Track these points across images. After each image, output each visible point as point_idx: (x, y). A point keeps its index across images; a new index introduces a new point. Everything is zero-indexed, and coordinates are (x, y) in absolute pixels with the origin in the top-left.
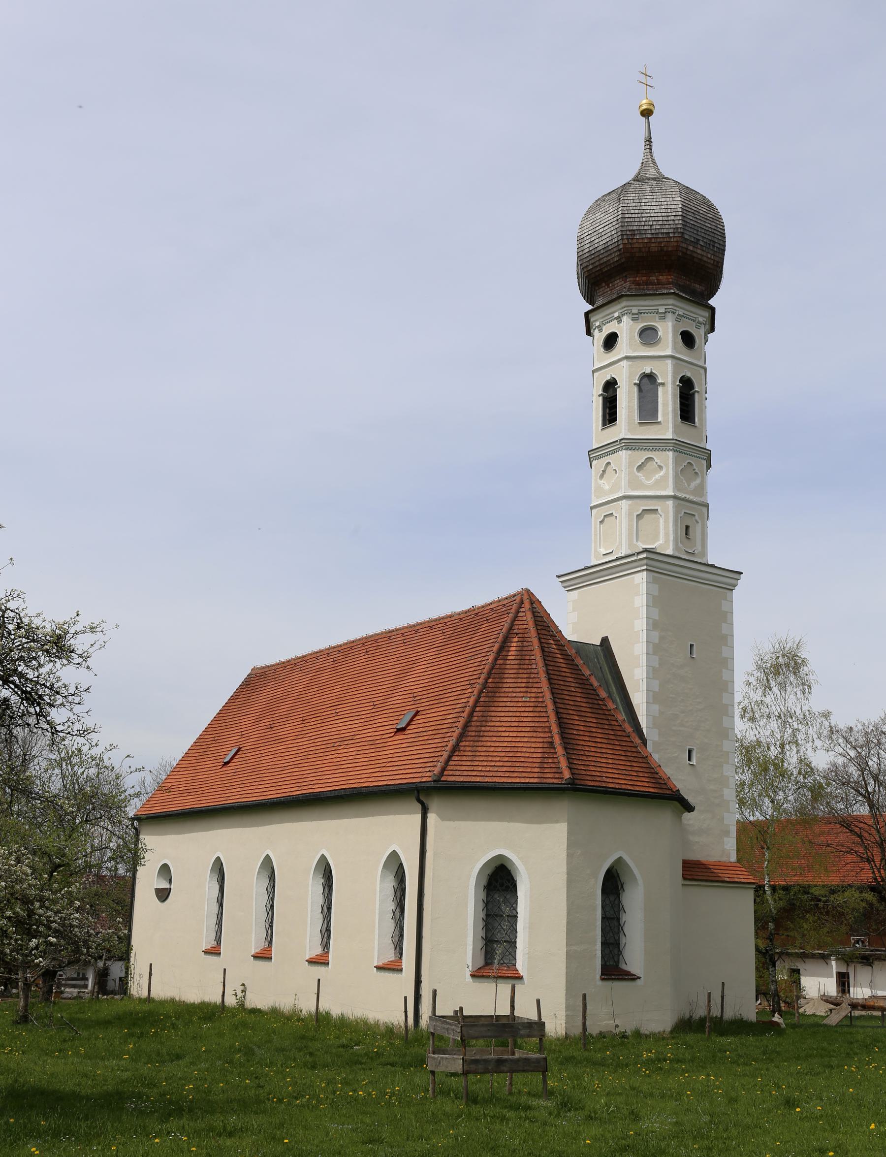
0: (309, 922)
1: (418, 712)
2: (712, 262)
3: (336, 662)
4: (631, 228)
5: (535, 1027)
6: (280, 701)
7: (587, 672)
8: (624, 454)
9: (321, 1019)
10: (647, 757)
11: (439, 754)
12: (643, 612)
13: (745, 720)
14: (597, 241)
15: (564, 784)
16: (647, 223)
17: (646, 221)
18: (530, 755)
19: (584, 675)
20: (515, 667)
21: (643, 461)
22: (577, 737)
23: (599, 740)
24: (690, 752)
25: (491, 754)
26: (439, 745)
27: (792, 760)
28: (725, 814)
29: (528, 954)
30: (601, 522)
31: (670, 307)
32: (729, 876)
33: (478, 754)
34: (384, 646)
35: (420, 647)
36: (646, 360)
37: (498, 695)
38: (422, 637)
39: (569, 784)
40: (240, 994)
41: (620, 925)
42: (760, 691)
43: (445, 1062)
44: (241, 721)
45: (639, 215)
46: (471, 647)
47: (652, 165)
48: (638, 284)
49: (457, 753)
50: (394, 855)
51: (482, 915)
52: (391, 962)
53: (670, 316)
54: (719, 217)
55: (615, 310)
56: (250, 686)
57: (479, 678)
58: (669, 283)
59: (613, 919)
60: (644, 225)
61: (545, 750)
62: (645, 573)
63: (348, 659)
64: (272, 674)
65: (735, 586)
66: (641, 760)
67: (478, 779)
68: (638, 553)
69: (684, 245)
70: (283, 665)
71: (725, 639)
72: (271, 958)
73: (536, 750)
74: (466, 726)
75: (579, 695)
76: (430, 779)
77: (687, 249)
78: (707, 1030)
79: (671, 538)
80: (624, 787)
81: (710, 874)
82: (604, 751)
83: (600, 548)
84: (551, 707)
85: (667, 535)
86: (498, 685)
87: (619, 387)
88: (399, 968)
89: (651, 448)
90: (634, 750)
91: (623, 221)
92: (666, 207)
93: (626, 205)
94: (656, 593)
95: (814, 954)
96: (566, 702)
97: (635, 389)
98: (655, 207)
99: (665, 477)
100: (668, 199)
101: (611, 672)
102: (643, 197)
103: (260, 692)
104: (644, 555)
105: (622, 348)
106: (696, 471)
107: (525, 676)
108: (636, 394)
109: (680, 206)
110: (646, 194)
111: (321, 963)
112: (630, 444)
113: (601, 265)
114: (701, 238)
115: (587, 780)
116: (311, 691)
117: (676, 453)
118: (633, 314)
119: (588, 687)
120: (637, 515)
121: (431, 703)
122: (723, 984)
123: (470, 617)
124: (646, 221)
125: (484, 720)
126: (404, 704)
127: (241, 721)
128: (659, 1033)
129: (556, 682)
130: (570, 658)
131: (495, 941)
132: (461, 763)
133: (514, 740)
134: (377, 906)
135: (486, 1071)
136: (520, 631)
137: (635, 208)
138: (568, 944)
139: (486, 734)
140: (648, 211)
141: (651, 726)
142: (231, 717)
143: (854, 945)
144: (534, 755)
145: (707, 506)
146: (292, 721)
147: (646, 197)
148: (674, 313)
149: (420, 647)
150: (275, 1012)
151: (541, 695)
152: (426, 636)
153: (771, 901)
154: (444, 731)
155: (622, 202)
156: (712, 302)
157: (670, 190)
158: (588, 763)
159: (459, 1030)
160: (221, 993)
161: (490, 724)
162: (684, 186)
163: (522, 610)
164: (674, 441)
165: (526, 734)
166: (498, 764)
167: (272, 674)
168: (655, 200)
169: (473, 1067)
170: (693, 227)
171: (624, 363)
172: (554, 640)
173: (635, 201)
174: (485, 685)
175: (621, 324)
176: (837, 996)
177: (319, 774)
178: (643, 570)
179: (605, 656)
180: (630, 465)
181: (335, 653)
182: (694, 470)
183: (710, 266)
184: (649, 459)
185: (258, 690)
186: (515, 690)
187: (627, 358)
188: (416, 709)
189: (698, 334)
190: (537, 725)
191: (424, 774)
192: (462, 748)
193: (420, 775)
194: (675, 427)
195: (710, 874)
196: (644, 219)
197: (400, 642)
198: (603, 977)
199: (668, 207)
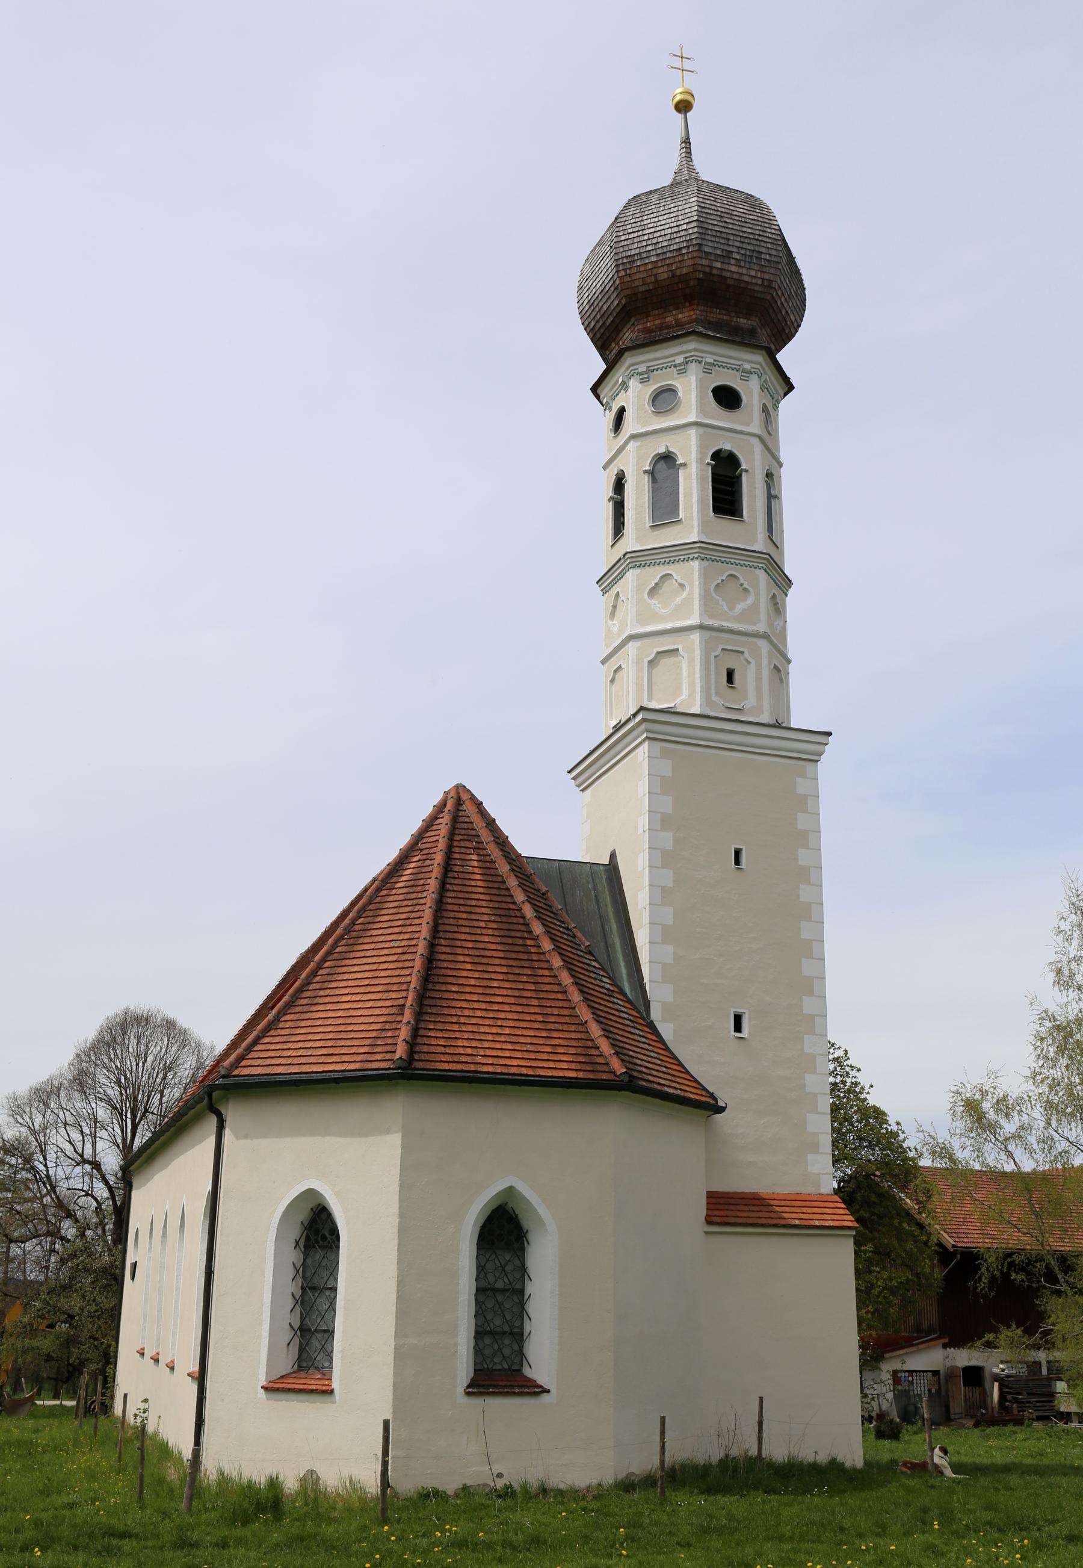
2: (760, 282)
4: (629, 253)
10: (586, 1022)
15: (393, 1069)
16: (649, 242)
17: (649, 239)
19: (514, 903)
21: (657, 580)
28: (807, 1115)
31: (692, 353)
36: (658, 435)
39: (399, 1068)
53: (692, 367)
60: (646, 246)
62: (646, 744)
65: (820, 754)
69: (705, 262)
77: (711, 267)
79: (698, 689)
85: (691, 685)
89: (667, 560)
92: (675, 214)
99: (688, 601)
106: (744, 586)
108: (647, 487)
114: (735, 250)
115: (441, 1061)
117: (705, 563)
120: (650, 662)
124: (649, 239)
138: (400, 1332)
140: (652, 225)
162: (714, 184)
170: (718, 234)
173: (635, 216)
178: (644, 740)
182: (742, 585)
183: (757, 288)
184: (667, 576)
194: (704, 526)
198: (470, 1390)
199: (680, 213)
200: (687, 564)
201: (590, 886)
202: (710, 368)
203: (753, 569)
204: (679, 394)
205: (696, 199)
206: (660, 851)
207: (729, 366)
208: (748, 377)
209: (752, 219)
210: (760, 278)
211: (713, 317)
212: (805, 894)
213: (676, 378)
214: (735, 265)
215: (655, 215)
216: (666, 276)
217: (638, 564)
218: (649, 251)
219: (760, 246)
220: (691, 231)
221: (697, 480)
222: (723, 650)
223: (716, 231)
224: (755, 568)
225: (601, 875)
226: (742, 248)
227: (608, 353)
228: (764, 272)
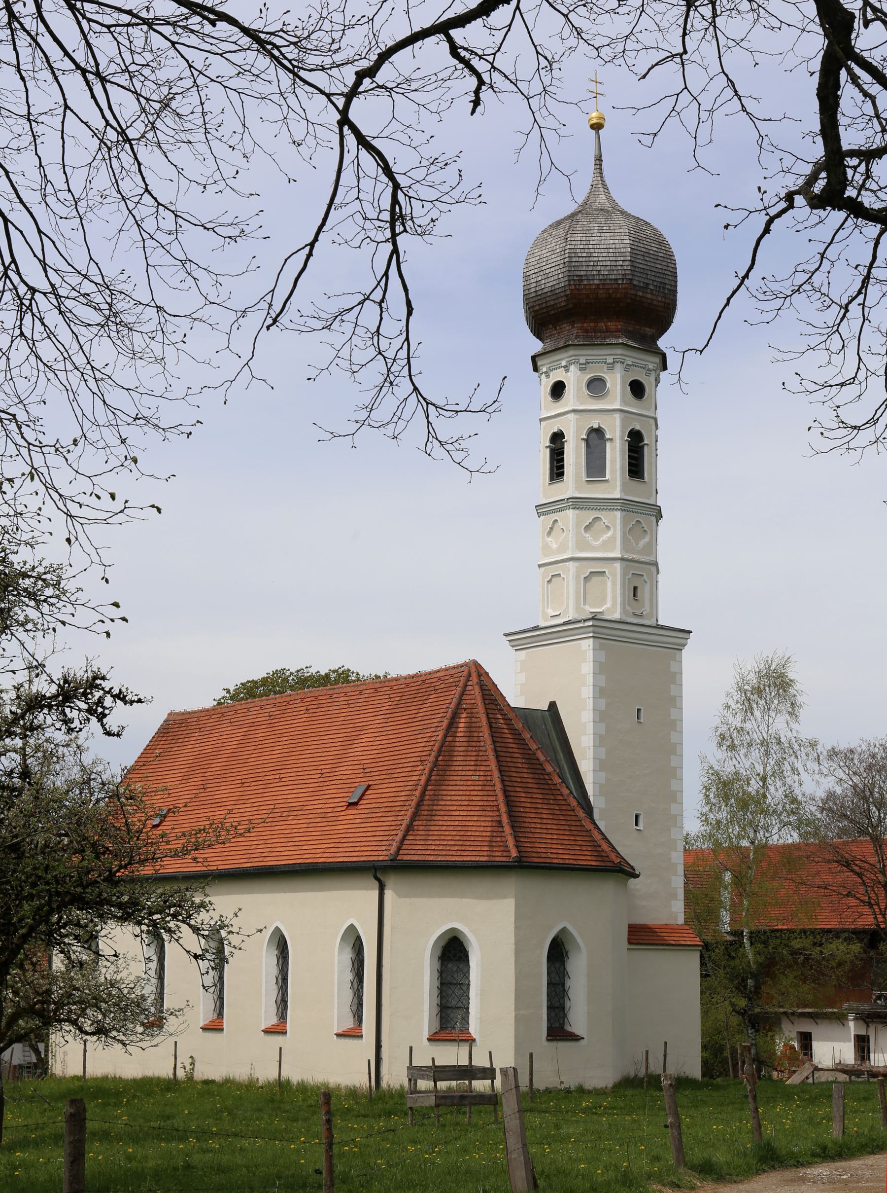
0: (264, 992)
1: (369, 786)
3: (272, 718)
4: (578, 273)
5: (488, 1071)
6: (211, 758)
7: (534, 747)
8: (571, 513)
9: (282, 1085)
11: (394, 832)
12: (590, 680)
13: (723, 749)
14: (543, 282)
16: (594, 268)
18: (481, 834)
19: (530, 749)
20: (465, 744)
21: (591, 521)
22: (524, 815)
23: (545, 816)
24: (637, 817)
25: (443, 833)
26: (393, 823)
27: (775, 794)
29: (480, 1018)
30: (549, 582)
31: (619, 357)
32: (675, 939)
33: (431, 833)
34: (325, 705)
35: (366, 711)
37: (448, 773)
38: (367, 700)
39: (516, 862)
40: (188, 1067)
41: (565, 990)
42: (739, 717)
43: (421, 1100)
44: (164, 777)
45: (587, 259)
46: (420, 719)
47: (602, 189)
48: (586, 331)
49: (411, 833)
50: (352, 928)
51: (437, 983)
52: (351, 1029)
53: (618, 366)
54: (671, 254)
55: (563, 358)
56: (170, 734)
57: (430, 755)
58: (618, 331)
59: (559, 984)
61: (494, 829)
62: (591, 640)
63: (286, 715)
64: (195, 723)
65: (684, 645)
66: (584, 834)
67: (432, 858)
68: (585, 621)
69: (633, 292)
70: (208, 713)
71: (674, 701)
72: (222, 1030)
73: (485, 829)
74: (419, 804)
75: (525, 771)
76: (387, 858)
77: (636, 295)
78: (645, 1084)
80: (567, 861)
81: (656, 938)
82: (549, 827)
83: (548, 608)
84: (499, 786)
86: (448, 763)
87: (566, 441)
88: (359, 1034)
90: (578, 823)
91: (570, 264)
93: (573, 247)
94: (603, 660)
95: (825, 1014)
96: (514, 779)
97: (583, 445)
98: (603, 250)
99: (613, 538)
100: (617, 242)
101: (559, 739)
102: (591, 238)
103: (183, 744)
104: (590, 623)
105: (572, 398)
107: (474, 754)
108: (583, 450)
109: (629, 250)
110: (594, 235)
111: (279, 1033)
112: (577, 503)
113: (547, 307)
116: (247, 749)
117: (624, 513)
118: (580, 364)
119: (534, 762)
120: (585, 578)
121: (383, 777)
122: (666, 1043)
123: (416, 684)
125: (436, 798)
126: (354, 776)
127: (164, 777)
128: (602, 1088)
129: (503, 759)
130: (517, 732)
131: (449, 1007)
132: (415, 842)
133: (464, 818)
134: (336, 977)
135: (453, 1105)
136: (469, 706)
137: (582, 251)
138: (517, 1008)
139: (438, 813)
141: (598, 794)
142: (151, 771)
143: (875, 1001)
144: (484, 834)
145: (656, 564)
146: (229, 783)
147: (594, 238)
148: (623, 363)
149: (366, 711)
150: (228, 1083)
151: (489, 773)
152: (372, 699)
153: (750, 956)
154: (397, 809)
155: (568, 243)
156: (663, 343)
157: (618, 231)
158: (533, 840)
159: (432, 1075)
160: (173, 1066)
161: (441, 803)
163: (469, 683)
164: (622, 501)
165: (476, 813)
166: (450, 843)
167: (195, 723)
168: (603, 242)
169: (443, 1101)
171: (571, 416)
172: (501, 715)
174: (435, 763)
175: (569, 374)
176: (855, 1064)
177: (269, 846)
179: (553, 722)
180: (578, 525)
181: (270, 706)
184: (597, 519)
185: (180, 741)
186: (464, 768)
187: (574, 411)
188: (367, 783)
189: (648, 382)
190: (486, 803)
191: (381, 853)
192: (415, 828)
193: (376, 853)
194: (623, 485)
195: (656, 938)
196: (592, 264)
197: (343, 703)
204: (608, 385)
205: (627, 237)
212: (674, 738)
220: (625, 268)
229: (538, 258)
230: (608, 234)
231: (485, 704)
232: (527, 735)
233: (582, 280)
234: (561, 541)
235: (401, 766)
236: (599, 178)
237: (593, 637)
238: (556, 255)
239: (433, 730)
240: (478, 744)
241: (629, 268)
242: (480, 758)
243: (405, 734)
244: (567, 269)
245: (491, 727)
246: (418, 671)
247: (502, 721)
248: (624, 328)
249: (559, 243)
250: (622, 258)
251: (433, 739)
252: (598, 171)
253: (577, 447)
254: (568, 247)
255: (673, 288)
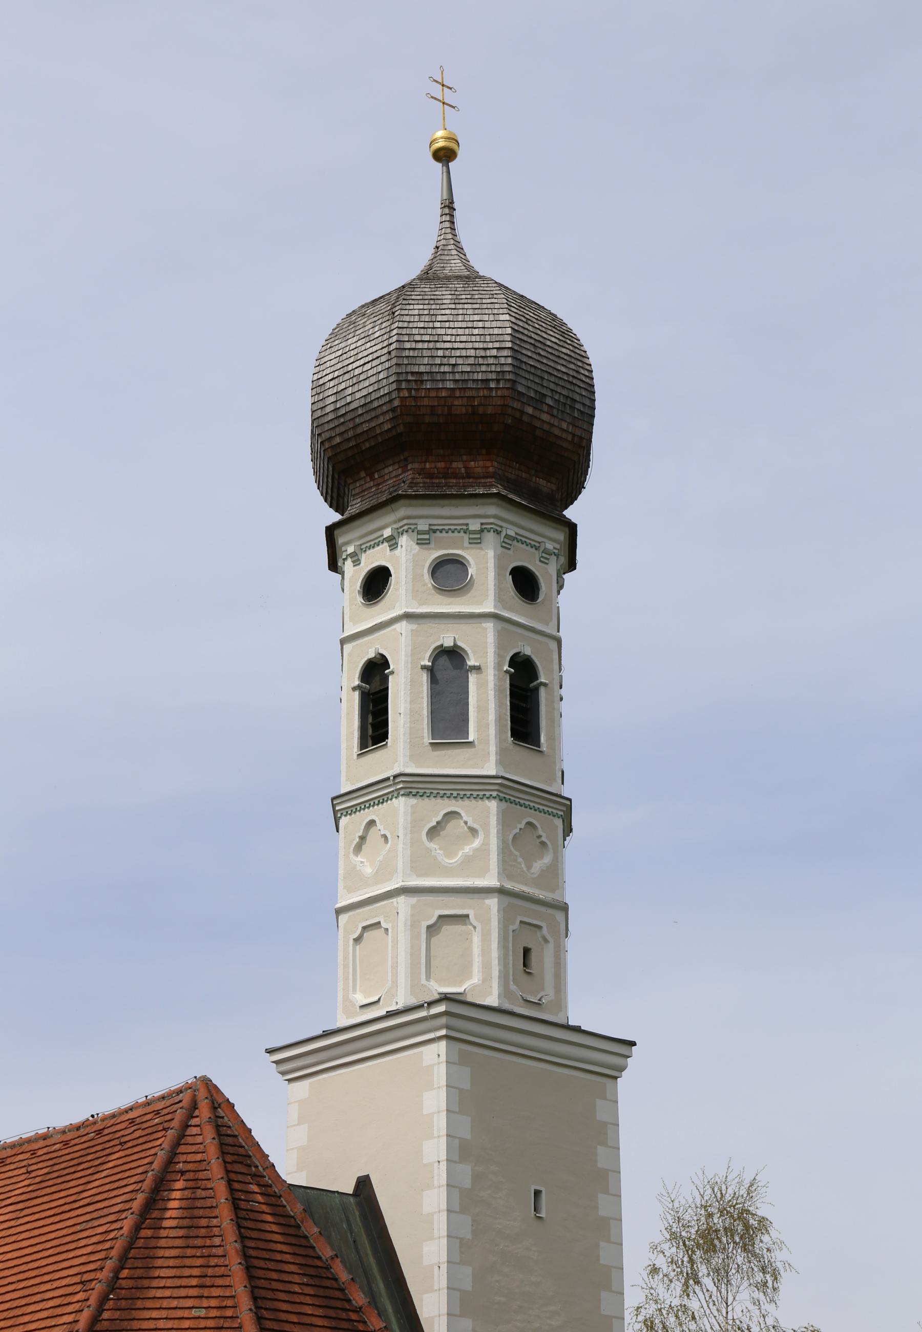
2: (570, 438)
4: (416, 369)
7: (326, 1252)
8: (401, 805)
12: (441, 1123)
14: (350, 391)
16: (445, 361)
17: (444, 357)
19: (319, 1258)
20: (178, 1243)
21: (439, 818)
30: (357, 940)
31: (491, 520)
37: (139, 1304)
42: (678, 1286)
47: (454, 252)
48: (430, 476)
53: (490, 537)
55: (385, 522)
60: (440, 365)
62: (443, 1044)
65: (622, 1069)
69: (516, 405)
75: (308, 1300)
77: (522, 412)
79: (495, 973)
83: (354, 991)
85: (486, 966)
87: (392, 673)
89: (455, 793)
93: (406, 325)
94: (467, 1086)
96: (283, 1316)
98: (460, 332)
99: (482, 852)
100: (486, 318)
104: (441, 1008)
107: (199, 1262)
108: (425, 688)
109: (509, 331)
114: (549, 393)
117: (504, 805)
118: (419, 533)
119: (328, 1283)
120: (429, 927)
124: (444, 357)
129: (261, 1273)
130: (292, 1222)
136: (190, 1167)
137: (422, 331)
147: (443, 312)
148: (499, 533)
151: (229, 1303)
157: (489, 301)
162: (515, 293)
163: (194, 1121)
164: (499, 781)
168: (460, 318)
170: (533, 370)
171: (403, 627)
172: (259, 1185)
174: (113, 1285)
175: (397, 552)
178: (440, 1038)
179: (364, 1216)
180: (414, 825)
182: (539, 837)
183: (565, 445)
184: (451, 815)
187: (408, 616)
189: (545, 573)
194: (502, 753)
196: (440, 353)
200: (480, 802)
201: (344, 1226)
202: (510, 542)
203: (551, 817)
204: (471, 571)
205: (505, 311)
206: (458, 1190)
207: (528, 541)
208: (548, 559)
209: (565, 354)
210: (571, 433)
211: (511, 473)
213: (467, 548)
214: (547, 413)
215: (452, 325)
216: (464, 411)
217: (414, 791)
218: (444, 373)
219: (574, 391)
220: (502, 361)
221: (495, 691)
222: (521, 922)
223: (531, 365)
224: (554, 816)
225: (353, 1209)
226: (556, 392)
227: (349, 481)
228: (576, 426)
229: (340, 353)
230: (469, 306)
231: (225, 1162)
232: (311, 1230)
233: (422, 381)
234: (381, 858)
235: (38, 1298)
236: (450, 236)
237: (446, 1037)
238: (373, 343)
239: (112, 1218)
240: (208, 1242)
241: (509, 361)
242: (210, 1272)
243: (52, 1236)
244: (394, 361)
245: (236, 1208)
246: (88, 1116)
247: (260, 1198)
248: (500, 472)
249: (379, 322)
250: (497, 345)
251: (112, 1235)
252: (447, 224)
253: (413, 682)
254: (396, 325)
255: (587, 411)
